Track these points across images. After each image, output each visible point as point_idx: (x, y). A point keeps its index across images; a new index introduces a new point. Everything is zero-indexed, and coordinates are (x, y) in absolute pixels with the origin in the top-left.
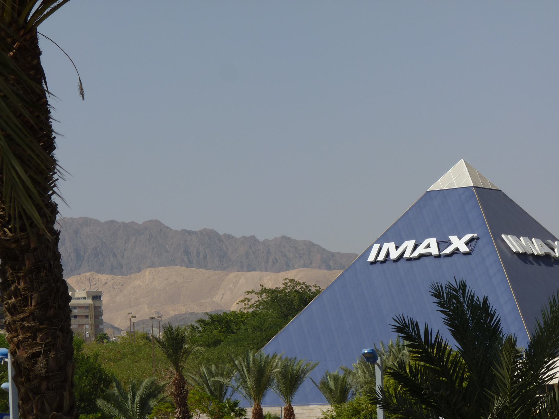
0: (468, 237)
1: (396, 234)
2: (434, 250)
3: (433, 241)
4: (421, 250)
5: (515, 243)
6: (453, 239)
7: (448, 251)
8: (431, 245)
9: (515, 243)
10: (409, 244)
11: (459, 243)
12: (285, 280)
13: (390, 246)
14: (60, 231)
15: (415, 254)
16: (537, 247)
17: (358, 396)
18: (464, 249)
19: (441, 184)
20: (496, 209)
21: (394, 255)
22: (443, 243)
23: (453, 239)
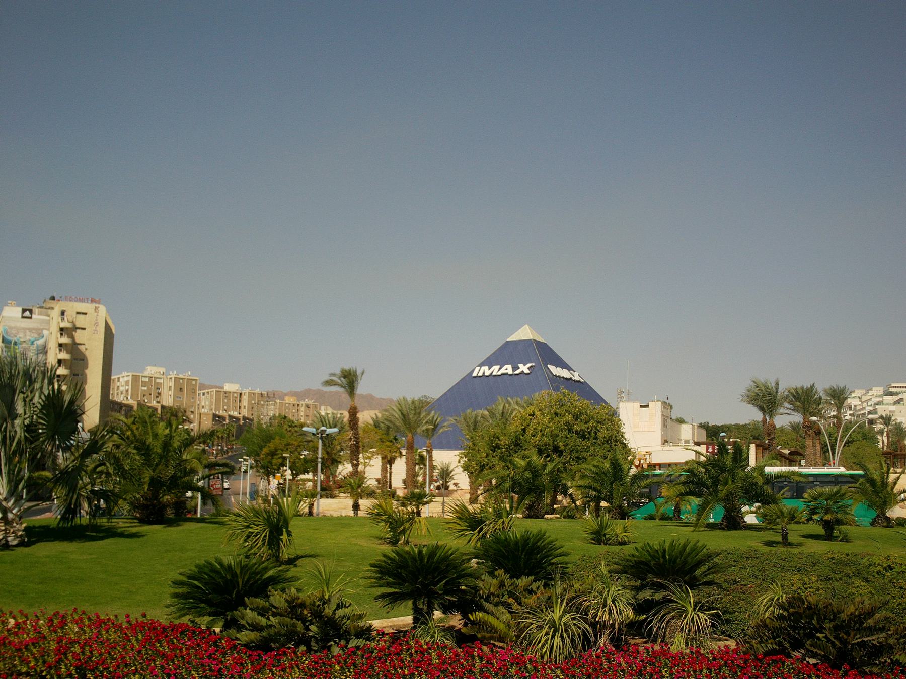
0: (529, 365)
1: (489, 362)
2: (510, 372)
3: (509, 367)
4: (503, 371)
5: (556, 371)
6: (521, 365)
7: (517, 372)
8: (508, 369)
9: (556, 371)
10: (496, 367)
11: (524, 368)
12: (902, 399)
13: (485, 368)
14: (701, 426)
15: (499, 373)
16: (565, 373)
17: (640, 641)
18: (527, 371)
19: (514, 337)
20: (545, 354)
21: (487, 373)
22: (515, 368)
23: (521, 365)
